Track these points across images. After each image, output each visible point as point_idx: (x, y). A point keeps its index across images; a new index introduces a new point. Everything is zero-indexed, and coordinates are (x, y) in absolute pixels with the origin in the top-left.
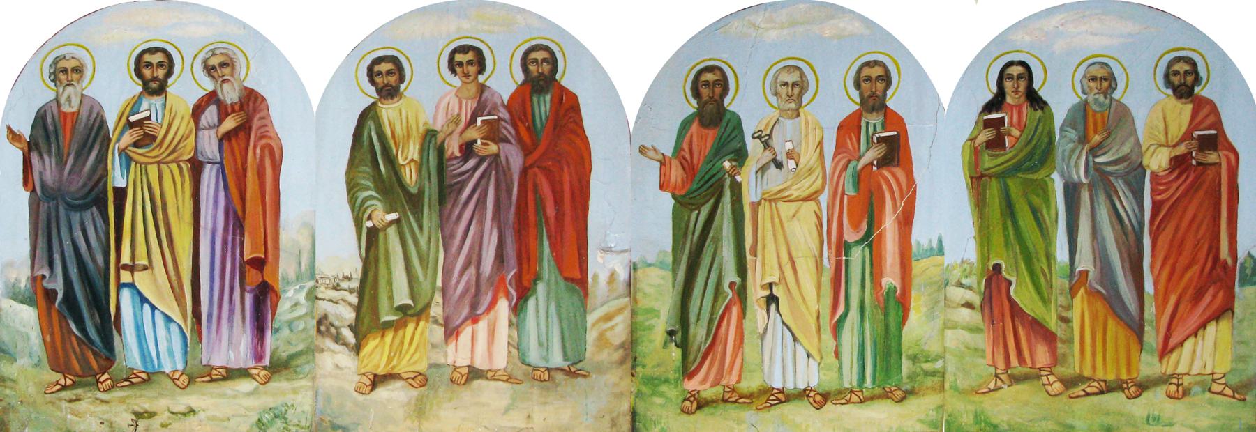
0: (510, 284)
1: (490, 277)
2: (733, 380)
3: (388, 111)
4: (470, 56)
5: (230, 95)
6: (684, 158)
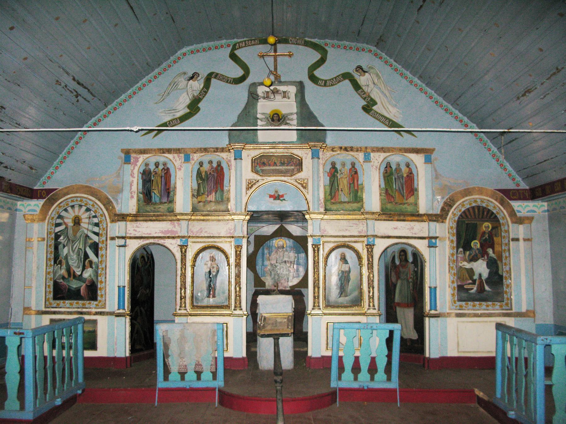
3: (201, 168)
5: (166, 168)
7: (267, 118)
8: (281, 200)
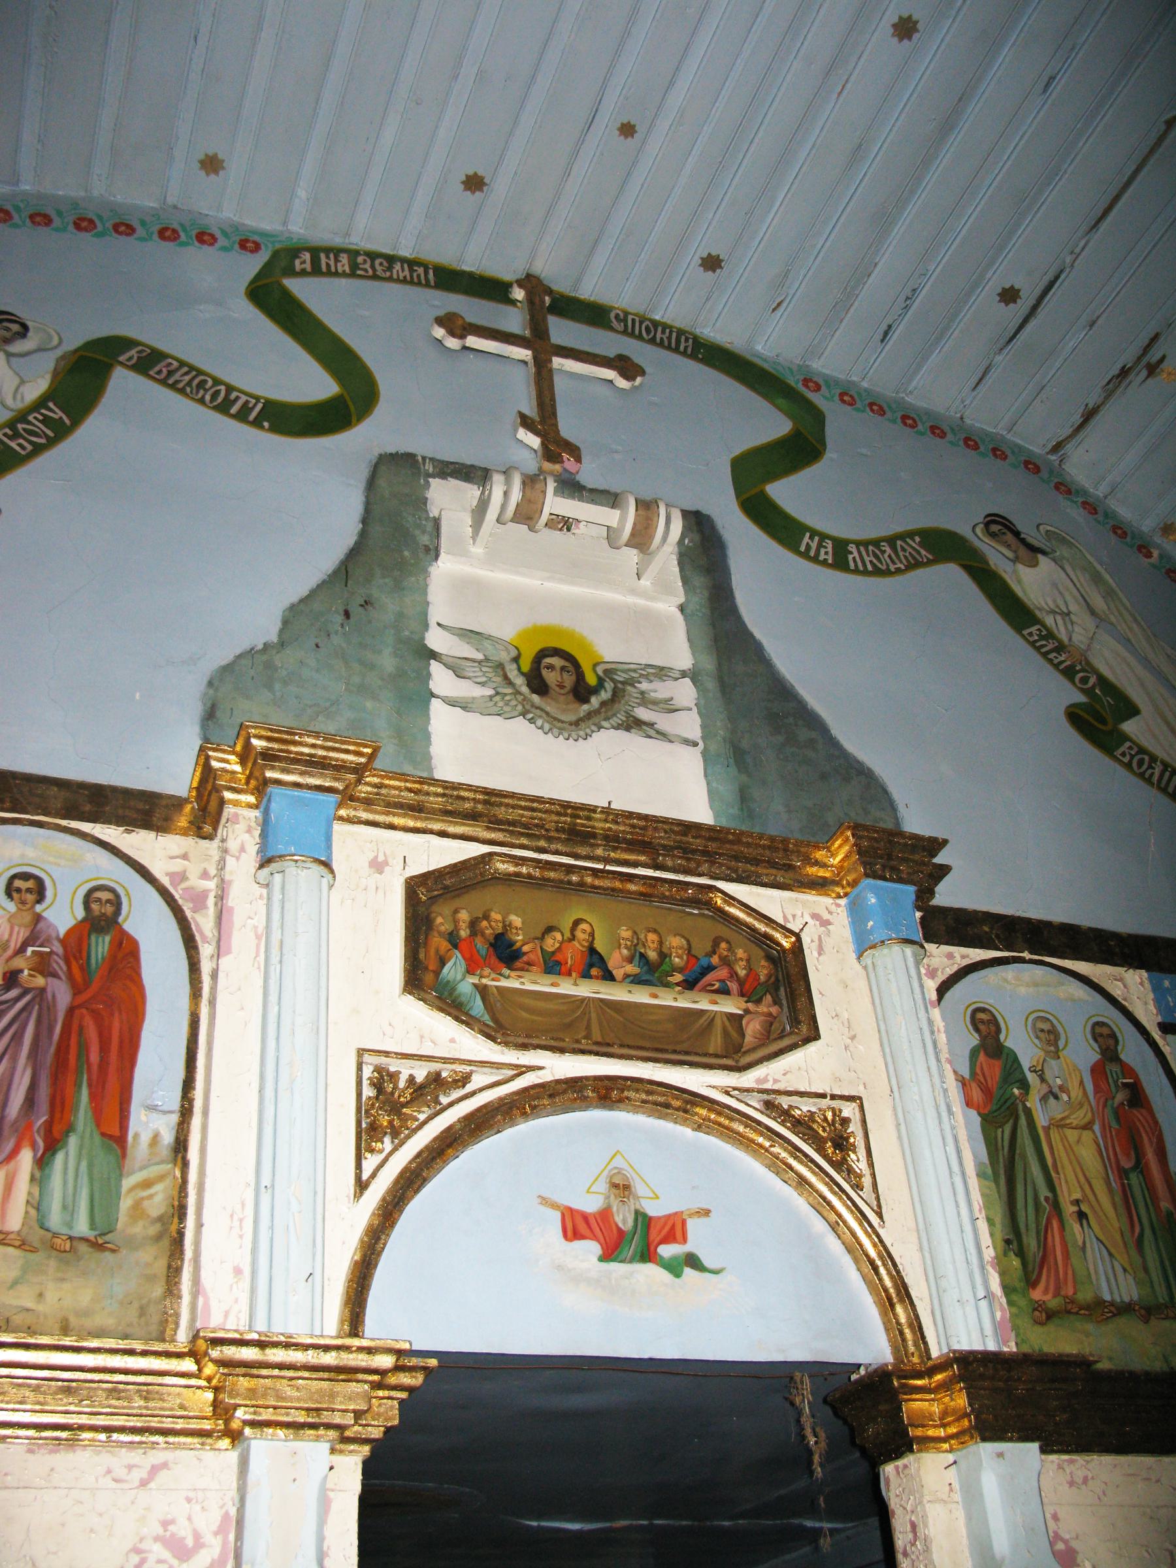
0: (38, 1131)
1: (16, 1121)
2: (1070, 1292)
4: (30, 884)
6: (980, 1081)
7: (500, 666)
8: (674, 1268)
